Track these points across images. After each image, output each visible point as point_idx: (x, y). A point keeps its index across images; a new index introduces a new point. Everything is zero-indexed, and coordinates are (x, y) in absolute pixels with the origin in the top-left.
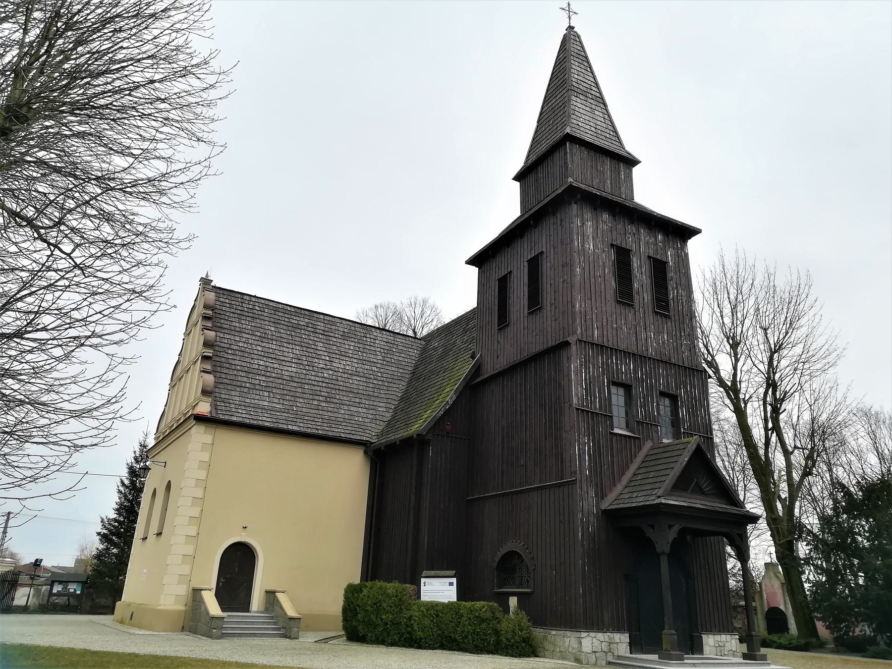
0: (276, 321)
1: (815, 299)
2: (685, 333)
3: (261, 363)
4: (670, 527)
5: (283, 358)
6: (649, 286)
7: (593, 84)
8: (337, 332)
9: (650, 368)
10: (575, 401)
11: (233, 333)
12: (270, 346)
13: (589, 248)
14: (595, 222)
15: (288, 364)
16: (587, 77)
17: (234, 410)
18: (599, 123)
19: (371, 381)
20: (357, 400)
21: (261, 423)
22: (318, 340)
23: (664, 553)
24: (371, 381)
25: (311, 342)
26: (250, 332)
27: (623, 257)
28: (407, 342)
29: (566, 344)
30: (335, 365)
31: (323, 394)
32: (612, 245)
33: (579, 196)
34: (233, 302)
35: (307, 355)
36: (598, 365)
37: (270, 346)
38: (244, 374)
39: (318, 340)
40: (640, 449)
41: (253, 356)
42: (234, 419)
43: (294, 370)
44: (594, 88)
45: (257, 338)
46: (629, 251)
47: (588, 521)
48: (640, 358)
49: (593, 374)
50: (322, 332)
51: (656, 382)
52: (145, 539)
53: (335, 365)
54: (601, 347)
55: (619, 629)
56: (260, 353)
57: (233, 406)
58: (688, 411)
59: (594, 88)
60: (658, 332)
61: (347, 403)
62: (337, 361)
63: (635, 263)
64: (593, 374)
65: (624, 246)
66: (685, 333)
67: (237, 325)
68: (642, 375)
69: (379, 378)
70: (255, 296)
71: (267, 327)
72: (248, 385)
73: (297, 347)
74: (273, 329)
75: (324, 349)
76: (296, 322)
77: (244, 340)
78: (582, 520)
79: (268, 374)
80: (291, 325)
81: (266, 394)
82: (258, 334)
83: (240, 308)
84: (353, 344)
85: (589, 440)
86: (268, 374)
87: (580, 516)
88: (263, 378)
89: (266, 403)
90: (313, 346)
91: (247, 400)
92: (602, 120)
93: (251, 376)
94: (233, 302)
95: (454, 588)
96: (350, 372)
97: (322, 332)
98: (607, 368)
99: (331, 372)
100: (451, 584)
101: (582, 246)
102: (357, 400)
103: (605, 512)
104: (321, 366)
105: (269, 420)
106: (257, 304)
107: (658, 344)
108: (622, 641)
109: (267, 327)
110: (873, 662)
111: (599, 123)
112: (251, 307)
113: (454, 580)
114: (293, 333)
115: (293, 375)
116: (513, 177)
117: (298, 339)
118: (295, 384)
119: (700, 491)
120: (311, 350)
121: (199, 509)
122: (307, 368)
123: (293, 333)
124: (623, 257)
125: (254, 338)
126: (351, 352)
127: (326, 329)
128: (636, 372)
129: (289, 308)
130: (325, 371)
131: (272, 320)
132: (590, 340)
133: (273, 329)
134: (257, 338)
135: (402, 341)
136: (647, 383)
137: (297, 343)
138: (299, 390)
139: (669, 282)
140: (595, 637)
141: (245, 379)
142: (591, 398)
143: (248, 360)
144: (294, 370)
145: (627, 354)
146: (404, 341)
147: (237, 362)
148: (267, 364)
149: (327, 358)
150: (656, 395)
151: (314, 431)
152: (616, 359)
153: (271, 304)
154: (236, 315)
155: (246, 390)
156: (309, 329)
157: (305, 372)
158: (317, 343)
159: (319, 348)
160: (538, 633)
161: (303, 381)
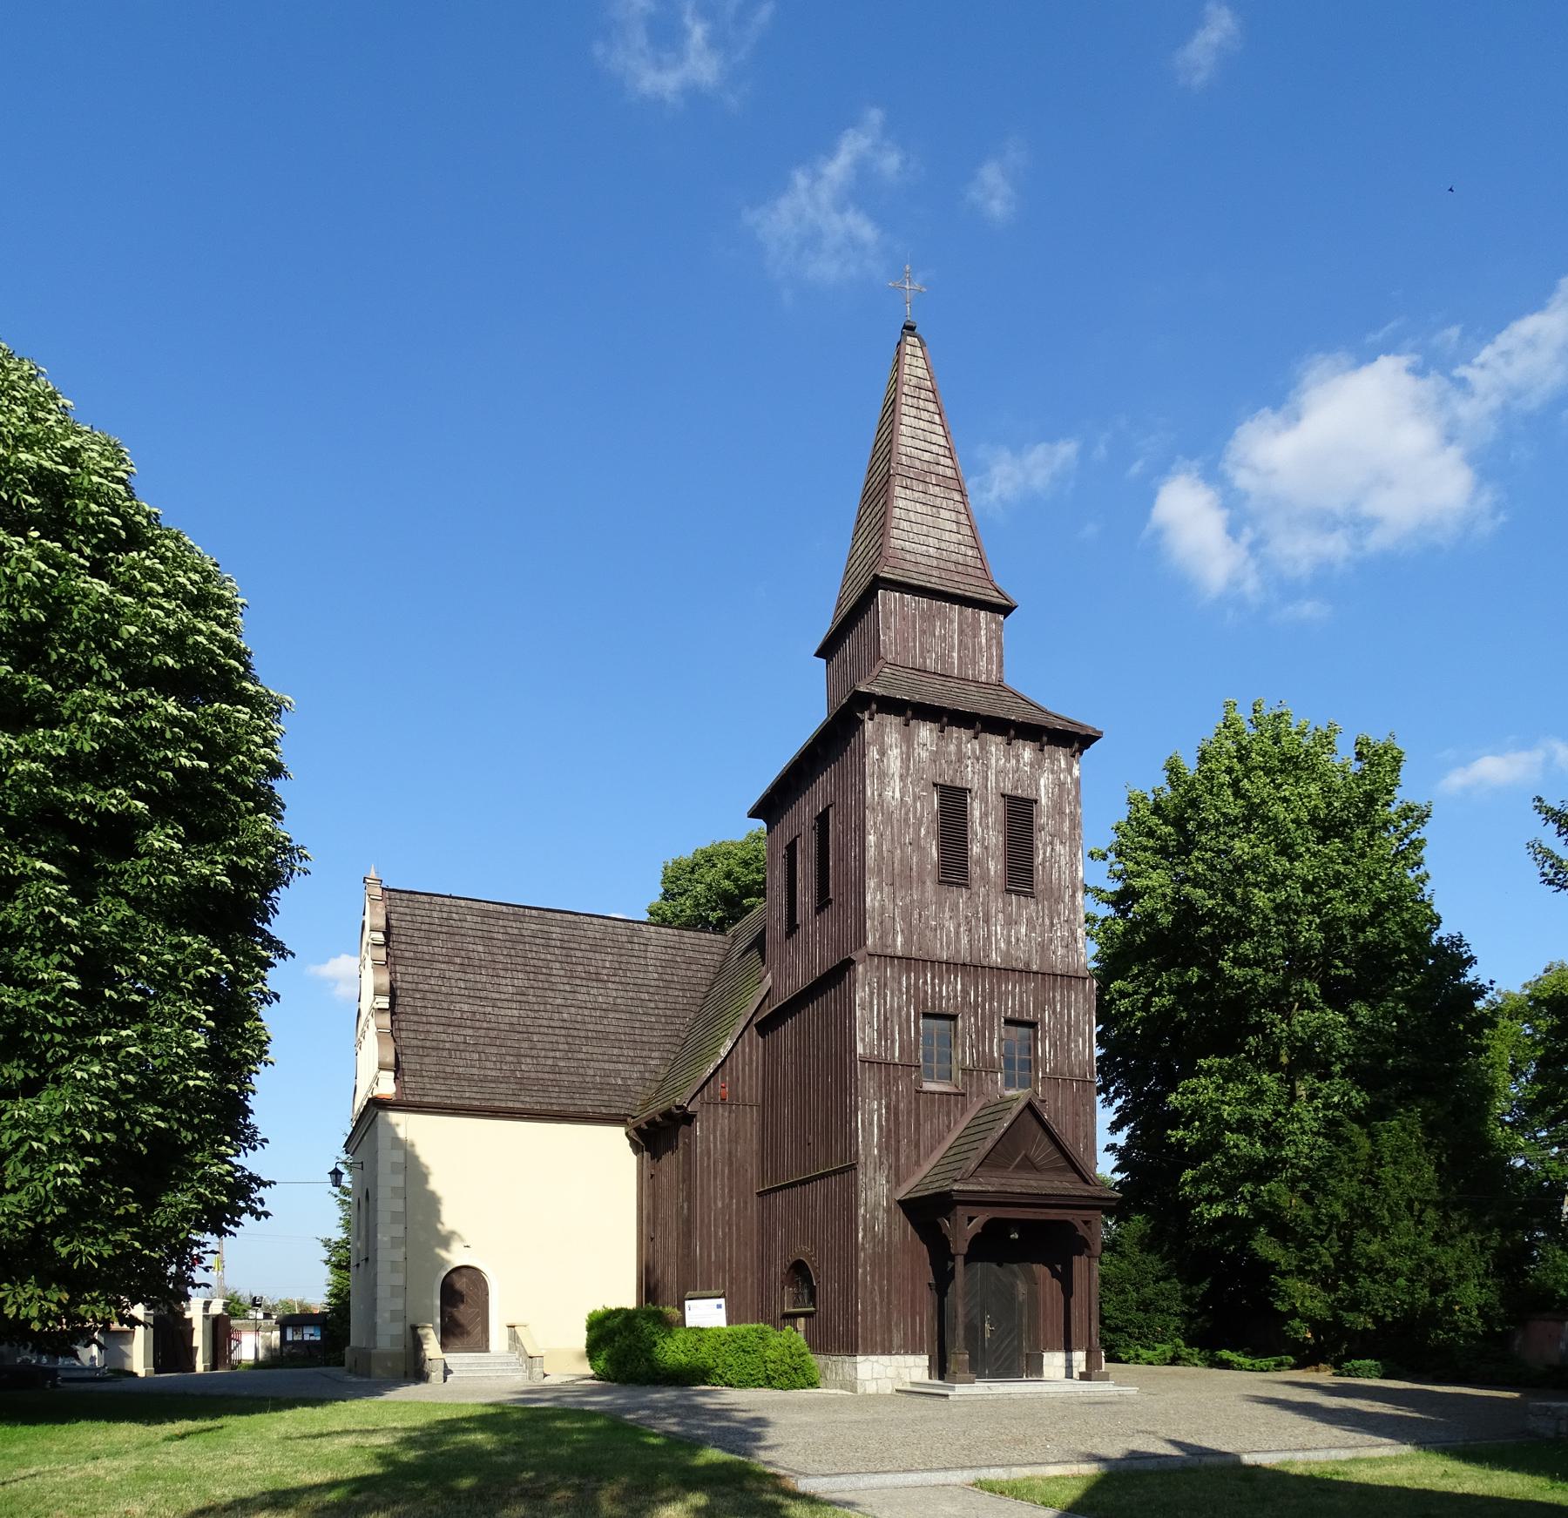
0: (485, 934)
1: (216, 1250)
2: (1059, 919)
3: (466, 1008)
4: (971, 1219)
5: (497, 996)
6: (1000, 852)
7: (941, 451)
8: (585, 940)
9: (991, 983)
10: (860, 1049)
11: (420, 963)
12: (478, 978)
13: (893, 798)
14: (904, 748)
15: (506, 1004)
16: (929, 437)
17: (428, 1086)
18: (946, 536)
19: (639, 1017)
20: (616, 1051)
21: (467, 1102)
22: (553, 958)
23: (34, 1319)
24: (639, 1017)
25: (540, 963)
26: (447, 959)
27: (953, 800)
28: (703, 942)
29: (848, 964)
30: (580, 997)
31: (561, 1047)
32: (935, 785)
33: (874, 707)
34: (417, 912)
35: (536, 986)
36: (900, 990)
37: (478, 978)
38: (441, 1029)
39: (553, 958)
40: (964, 1110)
41: (453, 998)
42: (426, 1099)
43: (516, 1013)
44: (942, 460)
45: (457, 968)
46: (964, 791)
47: (874, 1218)
48: (972, 969)
49: (892, 1006)
50: (558, 944)
51: (1000, 1006)
52: (358, 1265)
53: (580, 997)
54: (908, 962)
55: (915, 1350)
56: (463, 992)
57: (426, 1080)
58: (1053, 1045)
59: (942, 460)
60: (1010, 922)
61: (600, 1057)
62: (584, 990)
63: (975, 810)
64: (892, 1006)
65: (958, 783)
66: (1059, 919)
67: (425, 949)
68: (976, 996)
69: (651, 1011)
70: (450, 897)
71: (471, 947)
72: (448, 1045)
73: (521, 975)
74: (480, 949)
75: (562, 973)
76: (516, 931)
77: (437, 973)
78: (864, 1217)
79: (478, 1024)
80: (508, 937)
81: (476, 1056)
82: (458, 960)
83: (427, 920)
84: (610, 957)
85: (880, 1104)
86: (478, 1024)
87: (862, 1211)
88: (470, 1032)
89: (475, 1071)
90: (544, 970)
91: (448, 1069)
92: (954, 527)
93: (451, 1030)
94: (417, 912)
95: (723, 1311)
96: (604, 1006)
97: (558, 944)
98: (916, 994)
99: (573, 1010)
100: (719, 1306)
101: (880, 795)
102: (616, 1051)
103: (901, 1203)
104: (559, 1001)
105: (479, 1096)
106: (454, 909)
107: (1009, 943)
108: (915, 1368)
109: (471, 947)
110: (1175, 1373)
111: (946, 536)
112: (445, 915)
113: (722, 1301)
114: (513, 952)
115: (515, 1020)
116: (815, 650)
117: (520, 960)
118: (518, 1036)
119: (1028, 1165)
120: (541, 977)
121: (402, 1227)
122: (536, 1007)
123: (513, 952)
124: (953, 800)
125: (452, 968)
126: (605, 971)
127: (566, 938)
128: (965, 992)
129: (504, 909)
130: (564, 1010)
131: (479, 933)
132: (889, 951)
133: (480, 949)
134: (457, 968)
135: (693, 941)
136: (983, 1009)
137: (519, 968)
138: (525, 1045)
139: (1036, 835)
140: (877, 1362)
141: (443, 1037)
142: (886, 1041)
143: (445, 1005)
144: (516, 1013)
145: (953, 966)
146: (697, 941)
147: (430, 1011)
148: (476, 1008)
149: (568, 988)
150: (999, 1025)
151: (544, 1107)
152: (933, 979)
153: (476, 905)
154: (422, 934)
155: (445, 1054)
156: (538, 941)
157: (532, 1014)
158: (551, 964)
159: (555, 972)
160: (816, 1361)
161: (531, 1030)
